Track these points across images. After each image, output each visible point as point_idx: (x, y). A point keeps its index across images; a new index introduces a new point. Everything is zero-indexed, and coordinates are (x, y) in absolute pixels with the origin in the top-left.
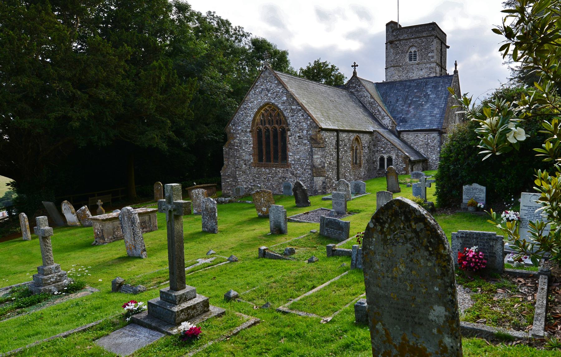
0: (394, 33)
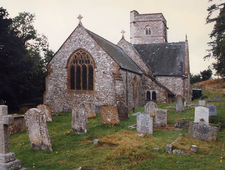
0: (136, 17)
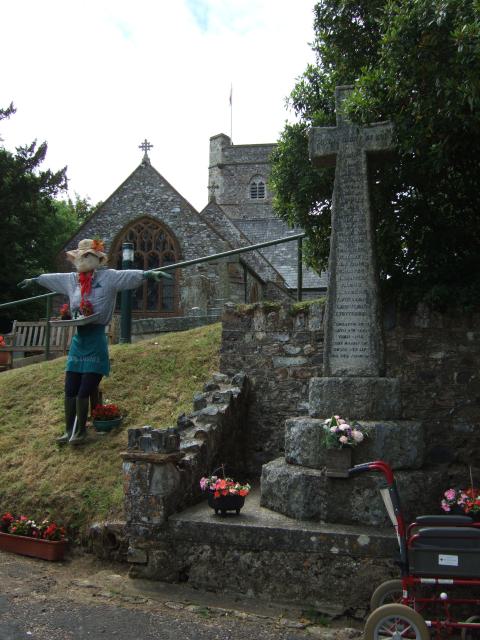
0: (226, 153)
